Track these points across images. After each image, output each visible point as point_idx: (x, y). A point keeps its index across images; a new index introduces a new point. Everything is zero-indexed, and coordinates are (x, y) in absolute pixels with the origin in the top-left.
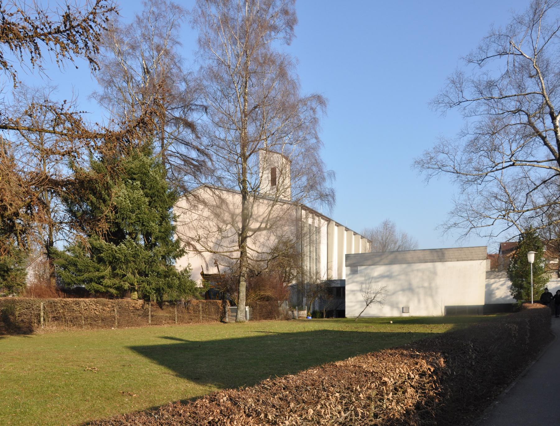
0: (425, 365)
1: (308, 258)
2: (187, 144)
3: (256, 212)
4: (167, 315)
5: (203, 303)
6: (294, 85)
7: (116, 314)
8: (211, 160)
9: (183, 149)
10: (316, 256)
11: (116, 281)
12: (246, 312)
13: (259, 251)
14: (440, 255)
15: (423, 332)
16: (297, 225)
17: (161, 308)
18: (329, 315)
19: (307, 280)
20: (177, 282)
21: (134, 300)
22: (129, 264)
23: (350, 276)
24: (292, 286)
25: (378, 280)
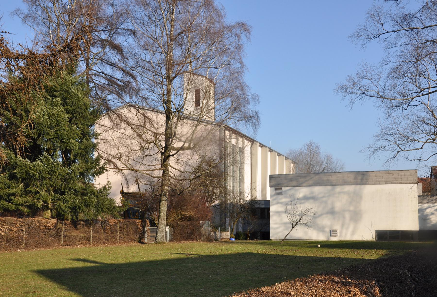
0: (359, 293)
1: (232, 178)
2: (112, 65)
3: (179, 132)
4: (82, 235)
5: (121, 223)
6: (219, 14)
7: (24, 235)
8: (136, 81)
9: (108, 70)
10: (240, 176)
11: (29, 199)
12: (166, 232)
13: (182, 170)
14: (362, 178)
15: (353, 257)
16: (220, 145)
17: (75, 227)
18: (253, 236)
19: (230, 200)
20: (95, 200)
21: (47, 219)
22: (44, 182)
23: (275, 197)
24: (215, 206)
25: (303, 201)
